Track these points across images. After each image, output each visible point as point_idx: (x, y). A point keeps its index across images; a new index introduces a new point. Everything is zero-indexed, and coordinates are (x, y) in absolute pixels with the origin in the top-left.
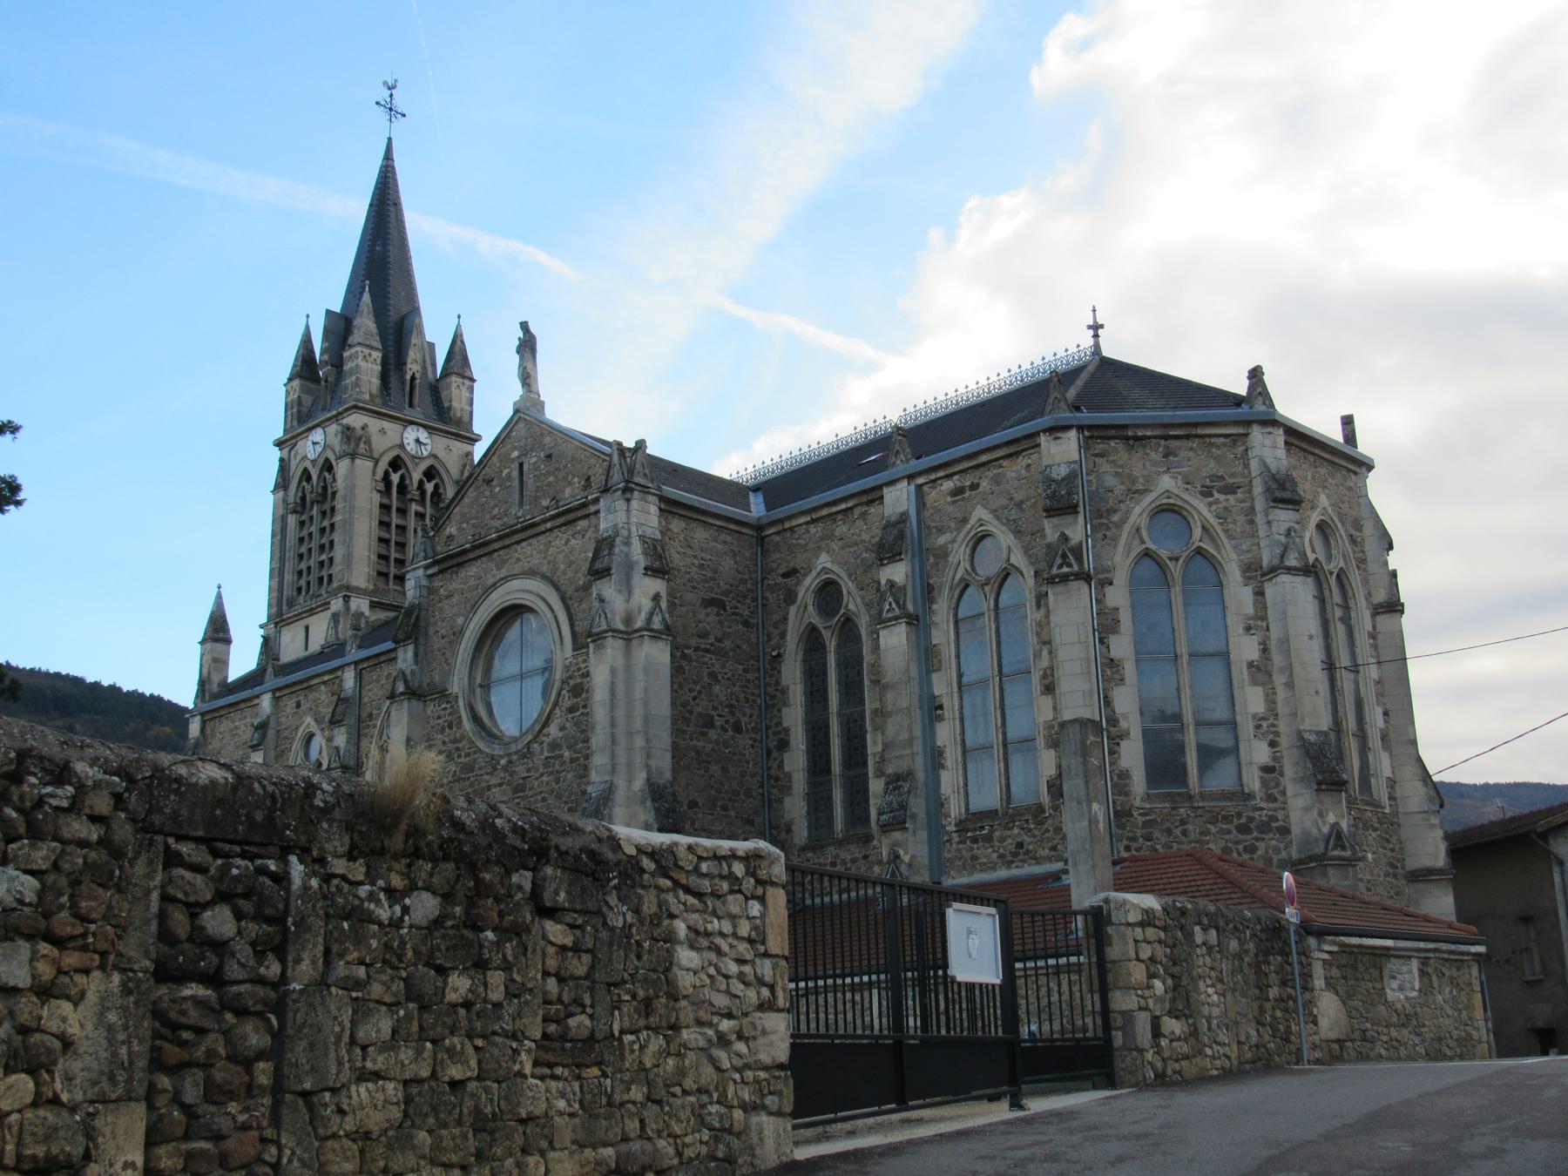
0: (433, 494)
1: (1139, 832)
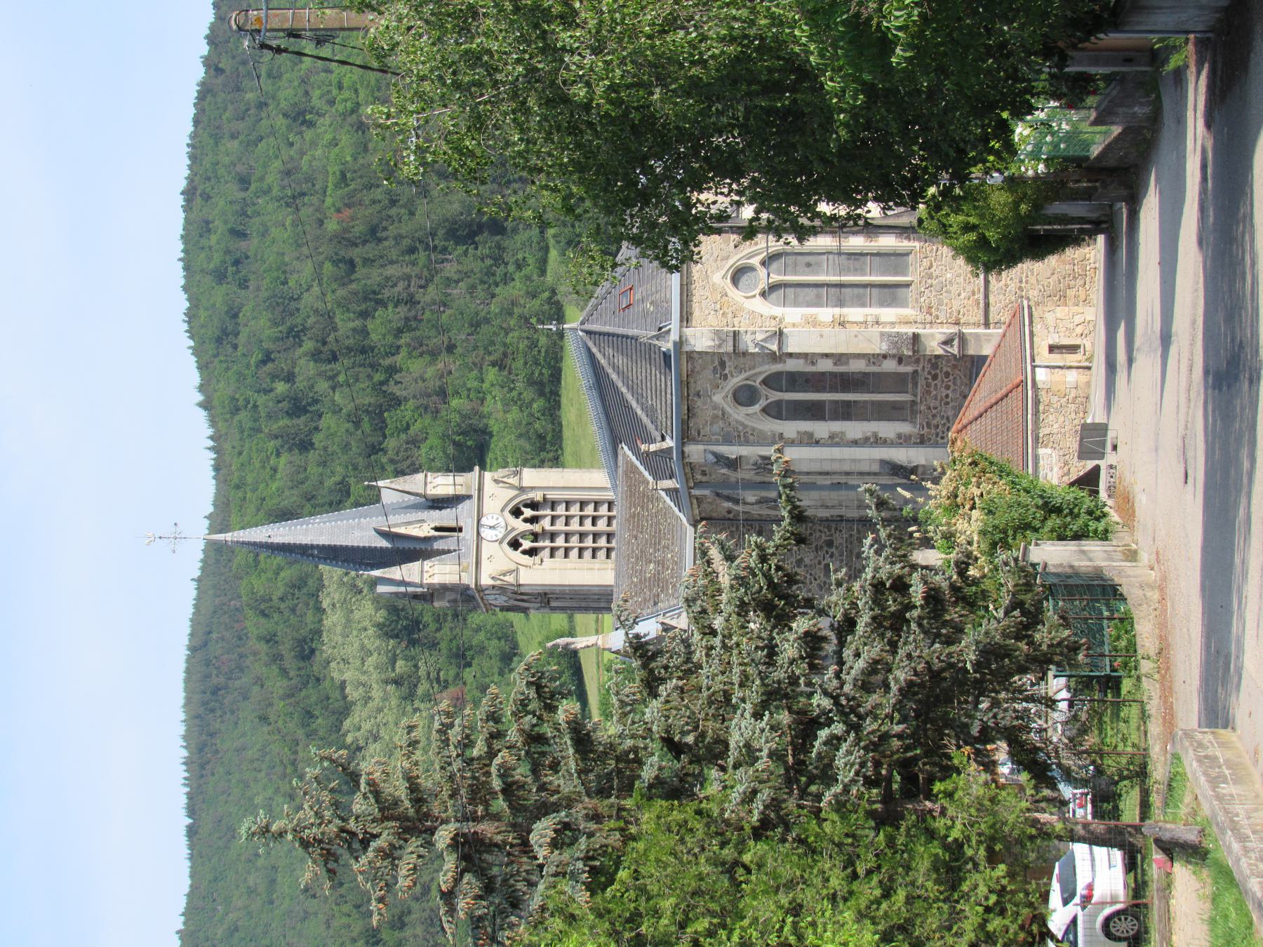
0: (533, 509)
1: (933, 431)
